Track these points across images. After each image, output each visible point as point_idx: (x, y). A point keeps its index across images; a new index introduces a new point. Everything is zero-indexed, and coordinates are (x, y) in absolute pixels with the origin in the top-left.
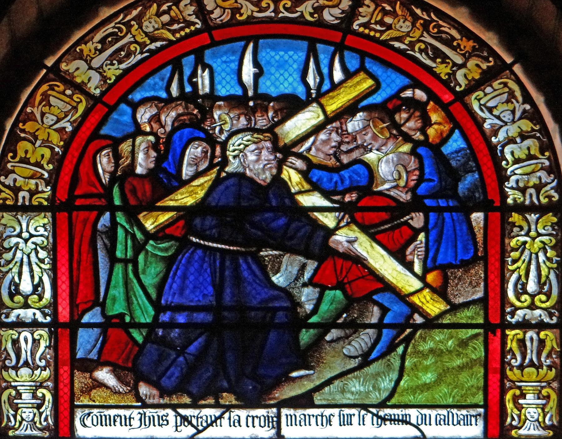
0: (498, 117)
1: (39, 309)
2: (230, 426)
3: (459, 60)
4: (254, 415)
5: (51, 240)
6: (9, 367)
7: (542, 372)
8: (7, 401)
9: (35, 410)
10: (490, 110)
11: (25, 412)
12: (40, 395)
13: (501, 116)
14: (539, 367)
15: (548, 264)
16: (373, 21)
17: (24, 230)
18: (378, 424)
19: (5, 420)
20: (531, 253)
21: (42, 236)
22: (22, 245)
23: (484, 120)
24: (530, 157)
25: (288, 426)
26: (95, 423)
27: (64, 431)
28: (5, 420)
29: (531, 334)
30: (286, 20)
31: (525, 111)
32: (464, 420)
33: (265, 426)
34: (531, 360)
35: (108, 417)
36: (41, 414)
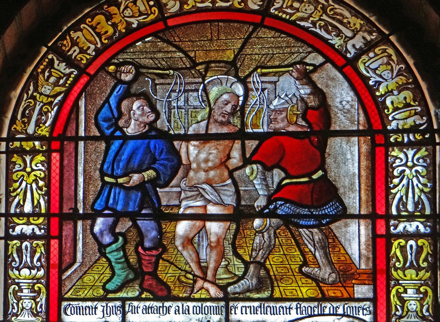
0: (380, 76)
1: (37, 225)
2: (242, 314)
3: (350, 34)
4: (247, 306)
5: (47, 172)
6: (14, 267)
7: (421, 273)
8: (12, 293)
9: (33, 301)
10: (374, 70)
11: (25, 303)
12: (36, 288)
13: (382, 74)
14: (419, 269)
15: (39, 192)
16: (284, 6)
17: (410, 159)
18: (163, 313)
19: (11, 307)
20: (27, 183)
21: (40, 170)
22: (408, 171)
23: (369, 78)
24: (407, 105)
25: (242, 314)
26: (73, 313)
27: (53, 317)
28: (11, 307)
29: (412, 242)
30: (221, 9)
31: (400, 70)
32: (305, 311)
33: (208, 313)
34: (412, 262)
35: (81, 307)
36: (37, 304)
